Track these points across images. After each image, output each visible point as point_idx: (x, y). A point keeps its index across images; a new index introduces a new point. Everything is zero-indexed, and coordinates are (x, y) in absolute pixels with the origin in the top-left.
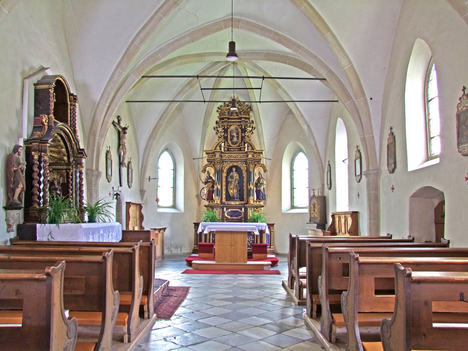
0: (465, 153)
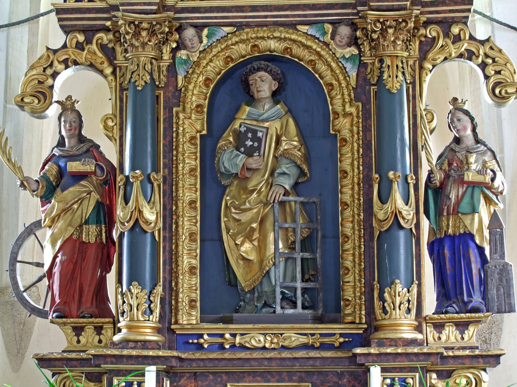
0: (447, 329)
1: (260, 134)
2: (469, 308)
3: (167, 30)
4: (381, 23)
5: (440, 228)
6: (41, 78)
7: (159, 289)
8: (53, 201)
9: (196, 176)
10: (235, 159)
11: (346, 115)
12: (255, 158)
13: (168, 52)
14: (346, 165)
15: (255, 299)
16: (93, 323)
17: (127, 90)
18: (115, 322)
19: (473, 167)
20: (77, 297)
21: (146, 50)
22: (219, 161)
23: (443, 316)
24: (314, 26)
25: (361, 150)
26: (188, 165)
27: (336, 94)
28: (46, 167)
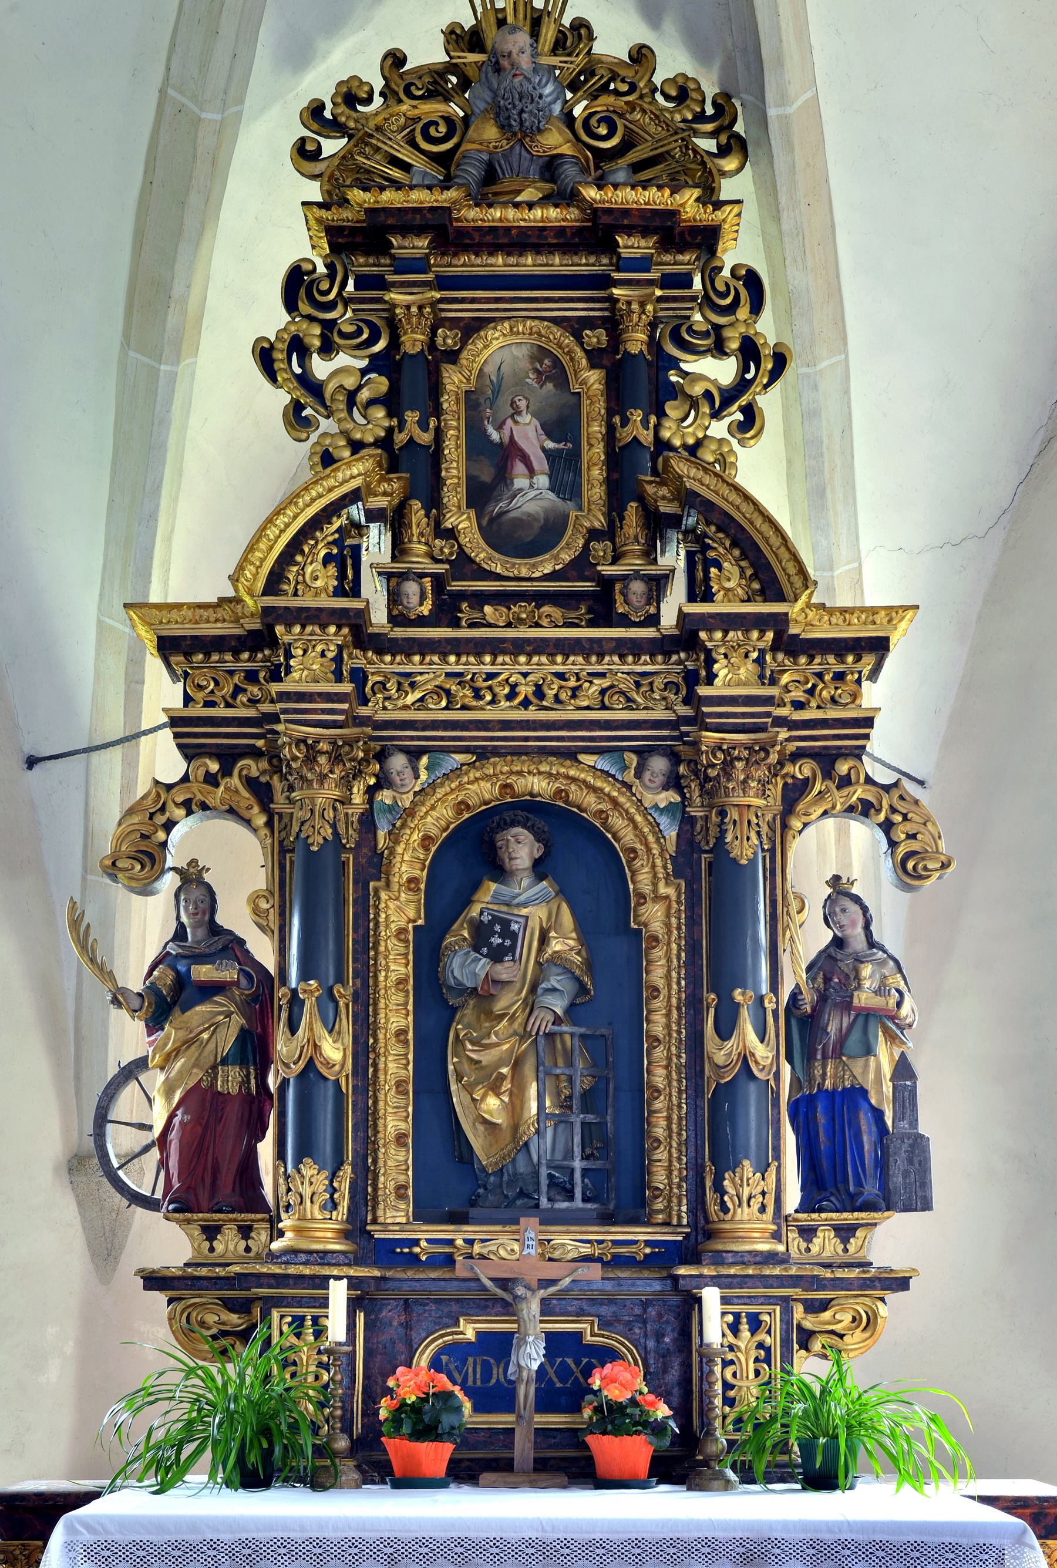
1: (515, 927)
2: (858, 1204)
3: (361, 755)
4: (723, 751)
5: (811, 1079)
6: (146, 829)
7: (348, 1169)
8: (167, 1026)
9: (407, 991)
10: (473, 965)
11: (657, 898)
12: (506, 964)
13: (361, 792)
14: (657, 976)
15: (504, 1186)
16: (235, 1220)
17: (292, 851)
18: (273, 1221)
19: (867, 984)
20: (208, 1180)
21: (326, 786)
22: (444, 968)
23: (815, 1216)
24: (607, 756)
25: (683, 954)
26: (393, 974)
27: (642, 865)
28: (155, 973)
